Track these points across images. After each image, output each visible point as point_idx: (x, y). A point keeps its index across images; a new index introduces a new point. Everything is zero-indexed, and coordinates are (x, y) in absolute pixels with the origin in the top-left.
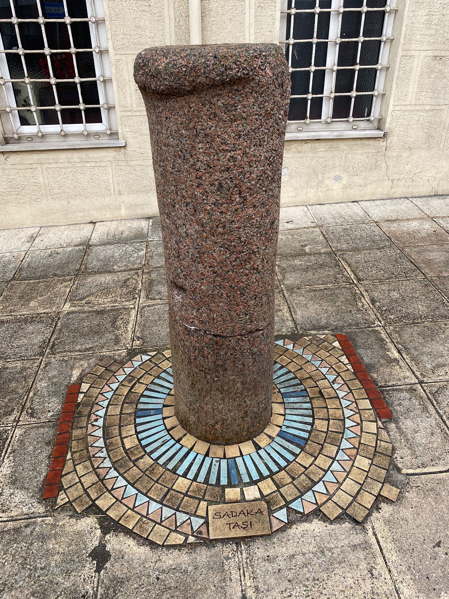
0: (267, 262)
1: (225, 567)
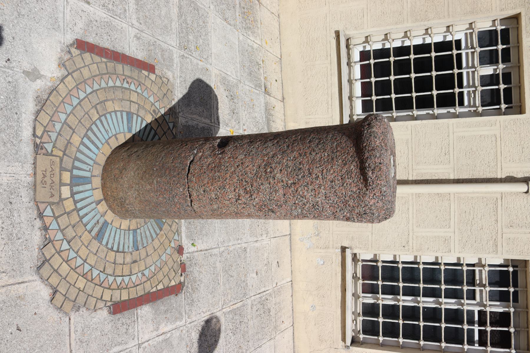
0: (244, 208)
1: (17, 163)
